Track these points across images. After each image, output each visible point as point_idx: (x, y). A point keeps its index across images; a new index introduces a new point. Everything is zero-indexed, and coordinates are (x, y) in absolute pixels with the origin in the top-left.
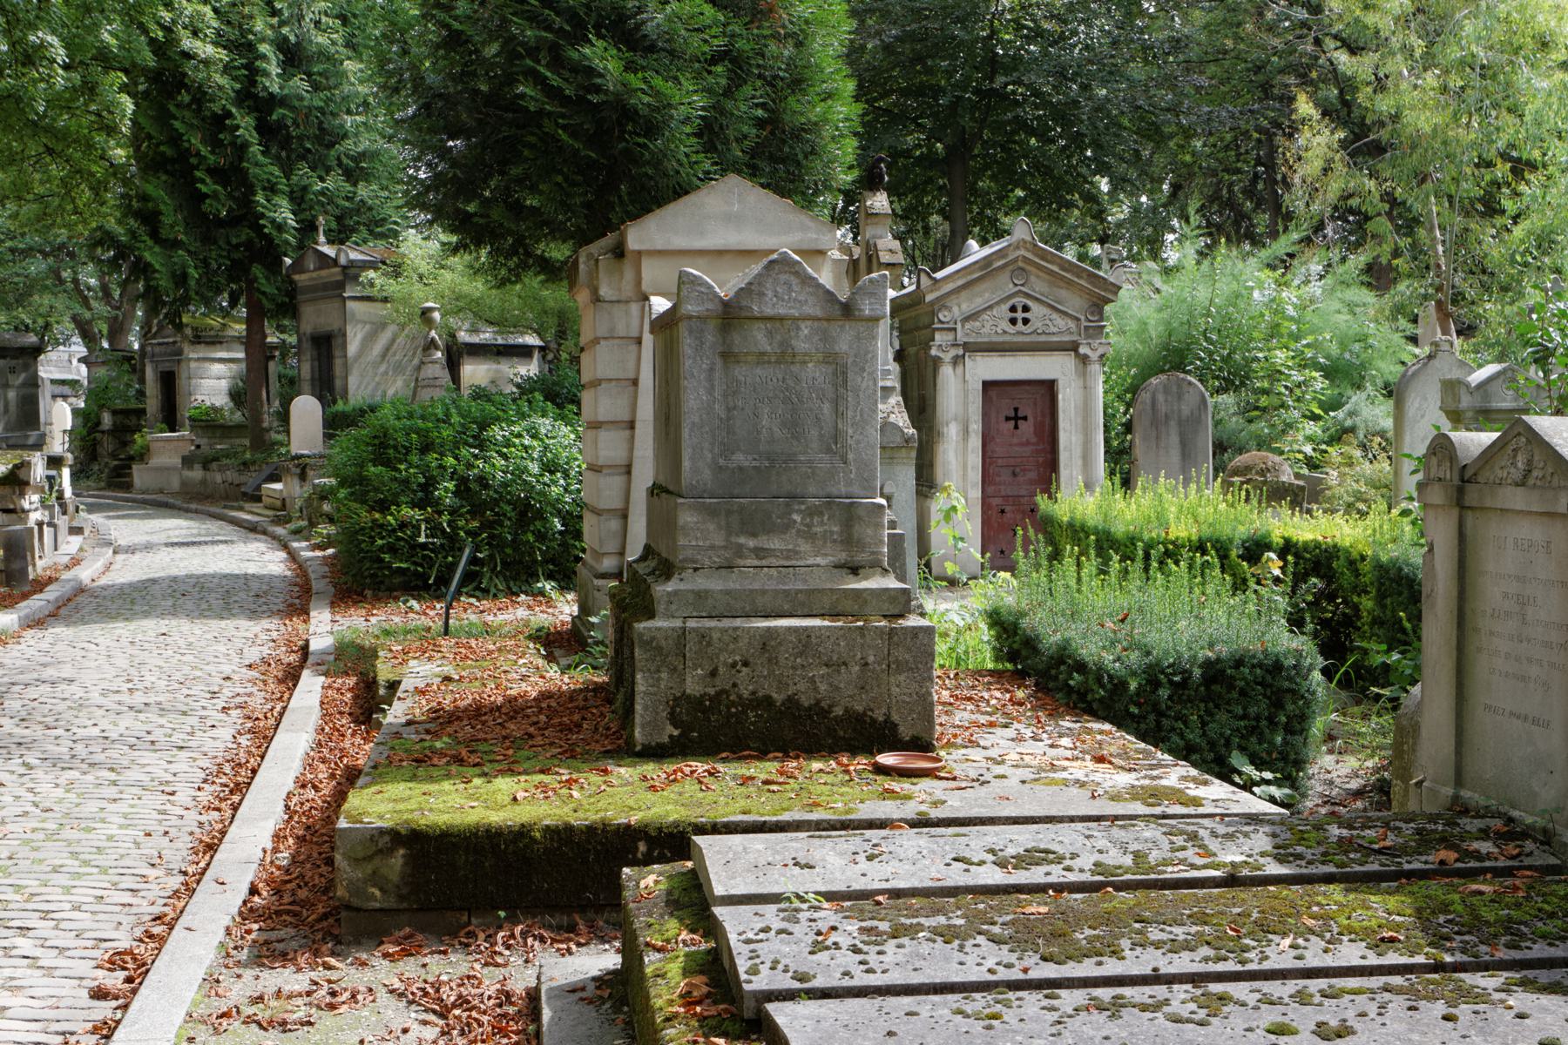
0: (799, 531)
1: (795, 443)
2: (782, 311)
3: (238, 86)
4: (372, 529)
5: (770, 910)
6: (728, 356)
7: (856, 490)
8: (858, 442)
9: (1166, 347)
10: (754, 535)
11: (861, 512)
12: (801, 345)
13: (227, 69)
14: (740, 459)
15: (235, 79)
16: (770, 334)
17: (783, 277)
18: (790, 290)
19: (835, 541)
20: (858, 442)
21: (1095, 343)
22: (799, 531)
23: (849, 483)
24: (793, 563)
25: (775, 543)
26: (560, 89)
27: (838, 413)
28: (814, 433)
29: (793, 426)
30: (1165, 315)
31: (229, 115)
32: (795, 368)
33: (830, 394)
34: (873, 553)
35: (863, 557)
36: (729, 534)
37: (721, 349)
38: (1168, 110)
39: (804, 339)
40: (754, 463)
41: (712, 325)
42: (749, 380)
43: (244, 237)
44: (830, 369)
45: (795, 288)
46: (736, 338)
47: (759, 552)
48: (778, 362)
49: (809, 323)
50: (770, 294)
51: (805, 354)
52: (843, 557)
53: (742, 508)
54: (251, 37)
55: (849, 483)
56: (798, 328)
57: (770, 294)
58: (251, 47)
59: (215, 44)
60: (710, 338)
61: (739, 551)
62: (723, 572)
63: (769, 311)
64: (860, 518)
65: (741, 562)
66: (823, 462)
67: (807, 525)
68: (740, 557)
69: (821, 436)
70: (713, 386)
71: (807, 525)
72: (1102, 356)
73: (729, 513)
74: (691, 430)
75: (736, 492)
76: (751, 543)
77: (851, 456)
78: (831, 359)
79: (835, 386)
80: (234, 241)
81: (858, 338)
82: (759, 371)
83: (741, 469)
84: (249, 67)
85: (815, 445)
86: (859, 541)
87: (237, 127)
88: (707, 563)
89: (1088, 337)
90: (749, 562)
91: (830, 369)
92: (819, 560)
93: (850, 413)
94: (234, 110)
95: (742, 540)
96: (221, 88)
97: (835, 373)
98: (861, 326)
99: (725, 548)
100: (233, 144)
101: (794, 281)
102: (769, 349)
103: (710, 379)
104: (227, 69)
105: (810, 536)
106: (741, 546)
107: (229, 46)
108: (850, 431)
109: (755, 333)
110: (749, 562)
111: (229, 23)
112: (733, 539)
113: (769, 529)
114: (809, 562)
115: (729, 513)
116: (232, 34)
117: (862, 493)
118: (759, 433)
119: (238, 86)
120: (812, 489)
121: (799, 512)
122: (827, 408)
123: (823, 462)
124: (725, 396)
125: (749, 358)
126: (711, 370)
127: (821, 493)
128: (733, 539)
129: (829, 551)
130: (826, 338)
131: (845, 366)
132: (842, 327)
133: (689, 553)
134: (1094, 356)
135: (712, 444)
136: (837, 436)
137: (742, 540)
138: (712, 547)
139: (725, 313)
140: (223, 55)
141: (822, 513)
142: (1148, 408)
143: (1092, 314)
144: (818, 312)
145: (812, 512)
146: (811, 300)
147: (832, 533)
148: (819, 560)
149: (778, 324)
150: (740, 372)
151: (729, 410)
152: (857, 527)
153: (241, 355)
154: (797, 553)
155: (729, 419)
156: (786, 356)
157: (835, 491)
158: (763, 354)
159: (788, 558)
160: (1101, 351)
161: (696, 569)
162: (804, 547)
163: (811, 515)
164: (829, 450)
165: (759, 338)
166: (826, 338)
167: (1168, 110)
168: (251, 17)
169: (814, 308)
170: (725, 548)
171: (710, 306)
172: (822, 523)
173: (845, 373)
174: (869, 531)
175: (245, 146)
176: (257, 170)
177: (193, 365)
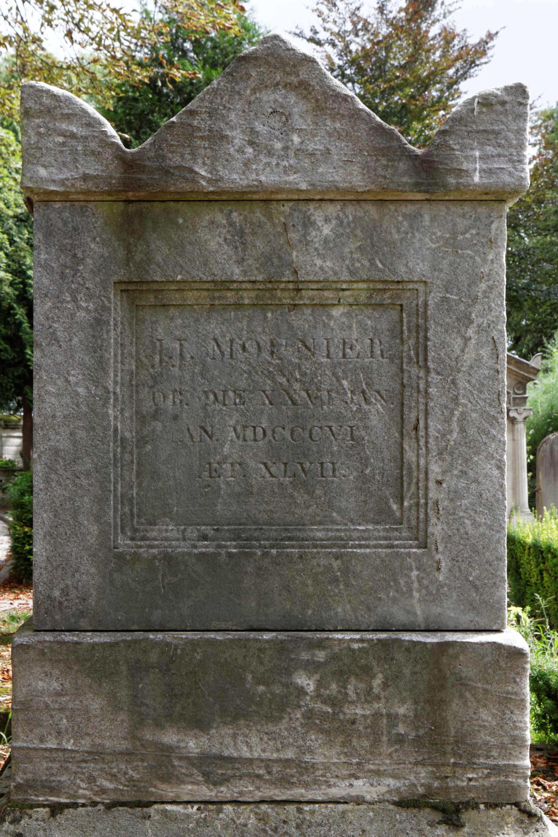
0: (309, 715)
1: (301, 497)
2: (267, 178)
3: (17, 293)
4: (24, 538)
5: (292, 808)
6: (139, 291)
7: (449, 611)
8: (455, 495)
9: (549, 416)
10: (200, 724)
11: (467, 669)
12: (315, 264)
13: (12, 284)
14: (169, 536)
15: (16, 289)
16: (239, 238)
17: (269, 98)
18: (287, 128)
19: (400, 740)
20: (455, 495)
21: (521, 409)
22: (309, 715)
23: (433, 595)
24: (298, 792)
25: (251, 744)
26: (360, 540)
27: (405, 426)
28: (347, 474)
29: (298, 455)
30: (548, 396)
31: (13, 308)
32: (301, 321)
33: (385, 381)
34: (496, 770)
35: (470, 780)
36: (139, 721)
37: (121, 274)
38: (523, 289)
39: (322, 249)
40: (205, 547)
41: (101, 214)
42: (190, 349)
43: (20, 372)
44: (384, 321)
45: (299, 122)
46: (159, 249)
47: (211, 767)
48: (260, 306)
49: (332, 209)
50: (238, 137)
51: (325, 285)
52: (420, 778)
53: (170, 657)
54: (24, 267)
55: (433, 595)
56: (308, 223)
57: (238, 137)
58: (24, 273)
59: (6, 271)
60: (94, 248)
61: (164, 764)
62: (123, 815)
63: (235, 178)
64: (462, 683)
65: (169, 791)
66: (368, 541)
67: (332, 701)
68: (167, 779)
69: (363, 479)
70: (101, 365)
71: (332, 701)
72: (525, 418)
73: (137, 669)
74: (51, 468)
75: (157, 616)
76: (193, 745)
77: (437, 529)
78: (389, 295)
79: (398, 360)
80: (16, 374)
81: (453, 243)
82: (214, 327)
83: (169, 559)
84: (25, 284)
85: (349, 503)
86: (460, 740)
87: (16, 314)
88: (84, 792)
89: (515, 405)
90: (187, 790)
91: (384, 321)
92: (360, 787)
93: (435, 426)
94: (15, 306)
95: (170, 737)
96: (7, 294)
97: (397, 333)
98: (460, 218)
99: (129, 755)
100: (14, 323)
101: (297, 105)
102: (237, 272)
103: (96, 348)
104: (12, 284)
105: (339, 729)
106: (167, 751)
107: (14, 273)
108: (435, 469)
109: (203, 235)
110: (187, 790)
111: (13, 261)
112: (148, 735)
113: (238, 709)
114: (336, 792)
115: (137, 669)
116: (14, 266)
117: (465, 620)
118: (214, 473)
119: (17, 293)
120: (342, 610)
121: (311, 667)
122: (377, 413)
123: (368, 541)
124: (133, 386)
125: (191, 296)
126: (99, 323)
127: (366, 619)
128: (148, 735)
129: (386, 764)
130: (374, 243)
131: (422, 312)
132: (413, 218)
133: (40, 768)
134: (520, 418)
135: (101, 501)
136: (402, 478)
137: (170, 737)
138: (97, 754)
139: (128, 184)
140: (9, 276)
141: (367, 672)
142: (548, 454)
143: (518, 389)
144: (357, 179)
145: (345, 667)
146: (340, 149)
147: (393, 719)
148: (360, 787)
149: (258, 214)
150: (167, 329)
151: (142, 419)
152: (455, 705)
153: (20, 434)
154: (306, 768)
155: (142, 441)
156: (279, 292)
157: (400, 616)
158: (224, 285)
159: (284, 781)
160: (525, 414)
161: (56, 810)
162: (324, 753)
163: (341, 676)
164: (382, 515)
165: (214, 246)
166: (374, 243)
167: (523, 289)
168: (25, 257)
169: (343, 170)
170: (129, 755)
171: (93, 168)
172: (369, 696)
173: (420, 331)
174: (486, 716)
175: (21, 323)
176: (27, 337)
177: (4, 439)
